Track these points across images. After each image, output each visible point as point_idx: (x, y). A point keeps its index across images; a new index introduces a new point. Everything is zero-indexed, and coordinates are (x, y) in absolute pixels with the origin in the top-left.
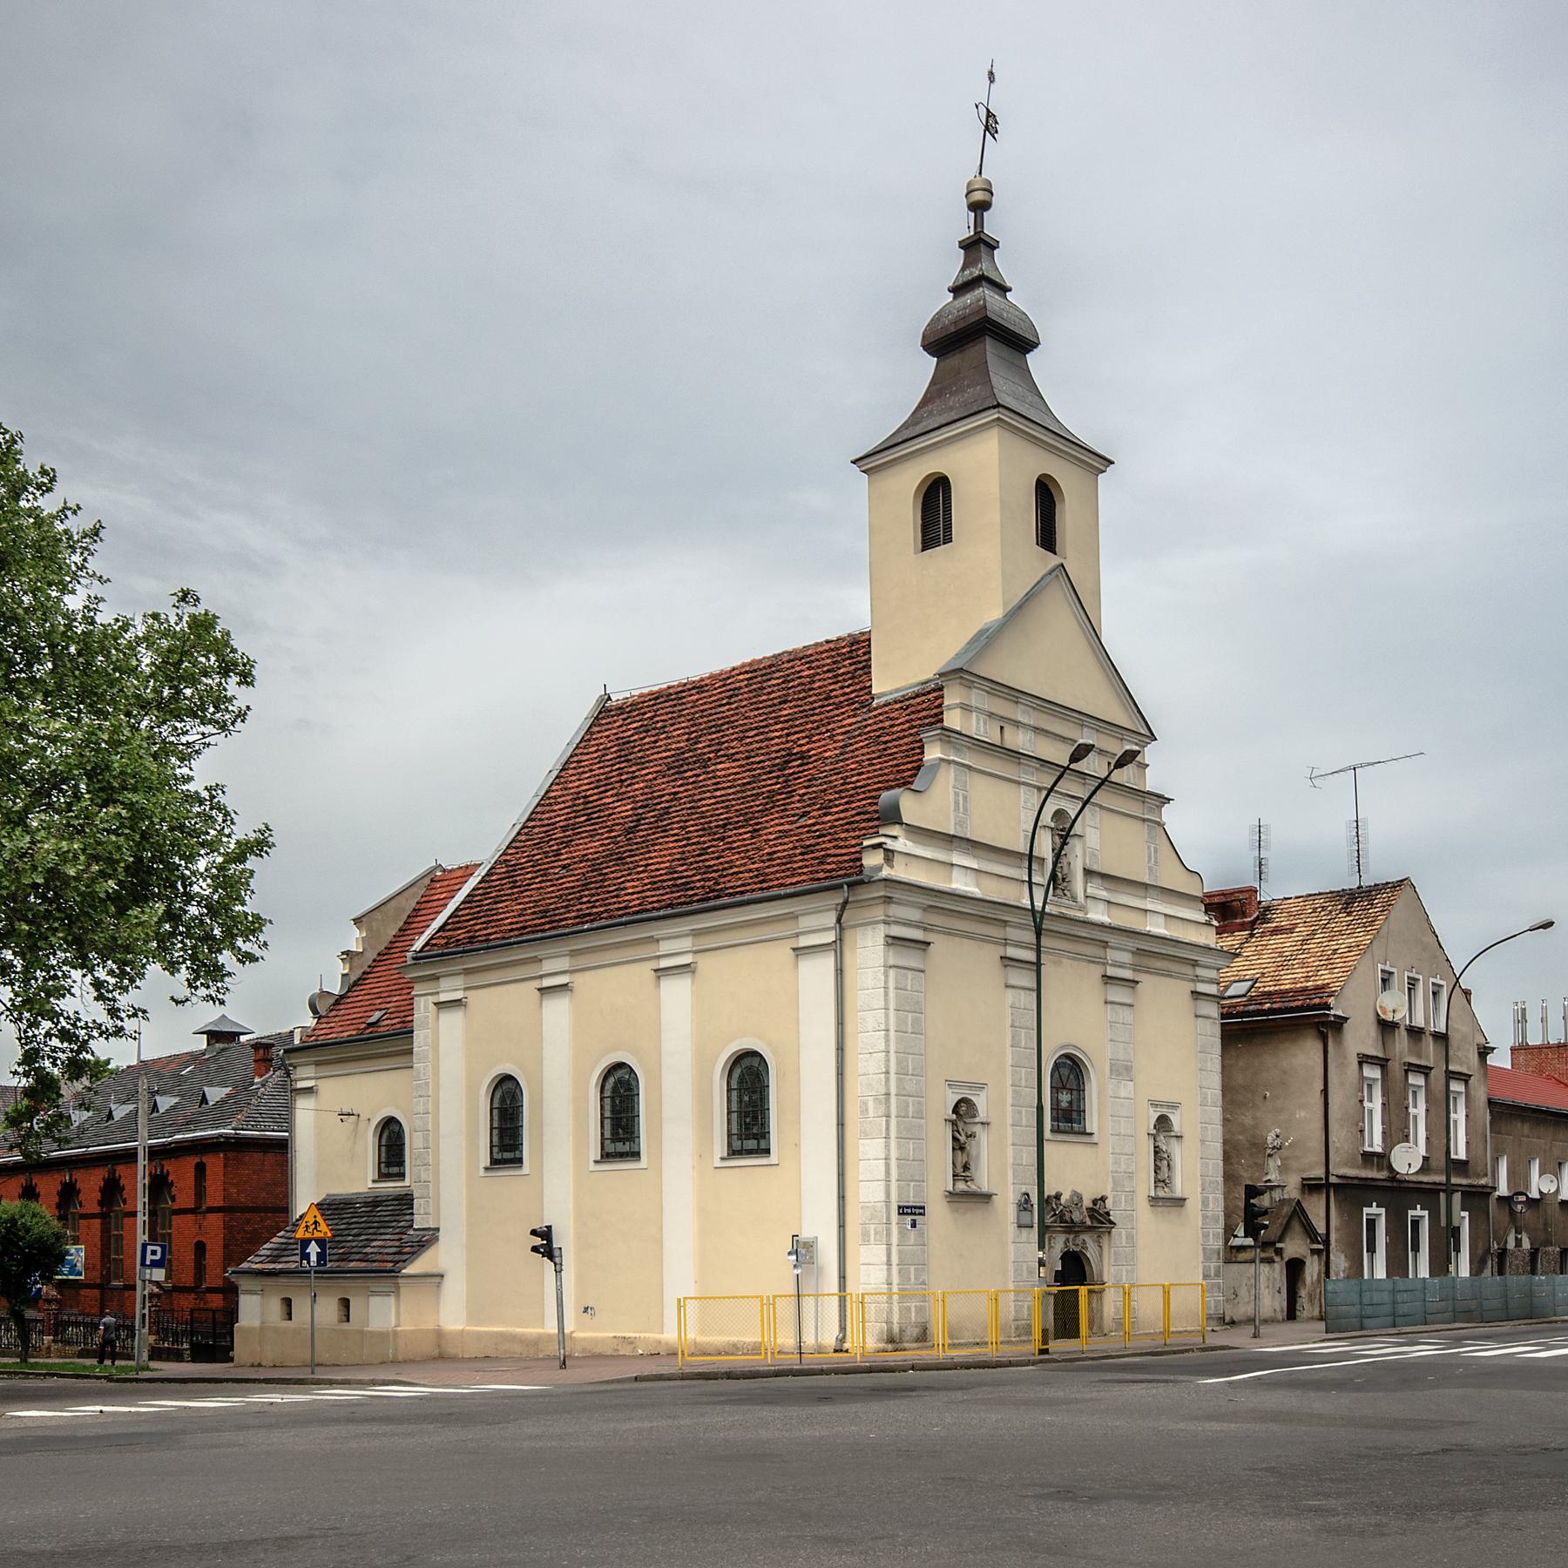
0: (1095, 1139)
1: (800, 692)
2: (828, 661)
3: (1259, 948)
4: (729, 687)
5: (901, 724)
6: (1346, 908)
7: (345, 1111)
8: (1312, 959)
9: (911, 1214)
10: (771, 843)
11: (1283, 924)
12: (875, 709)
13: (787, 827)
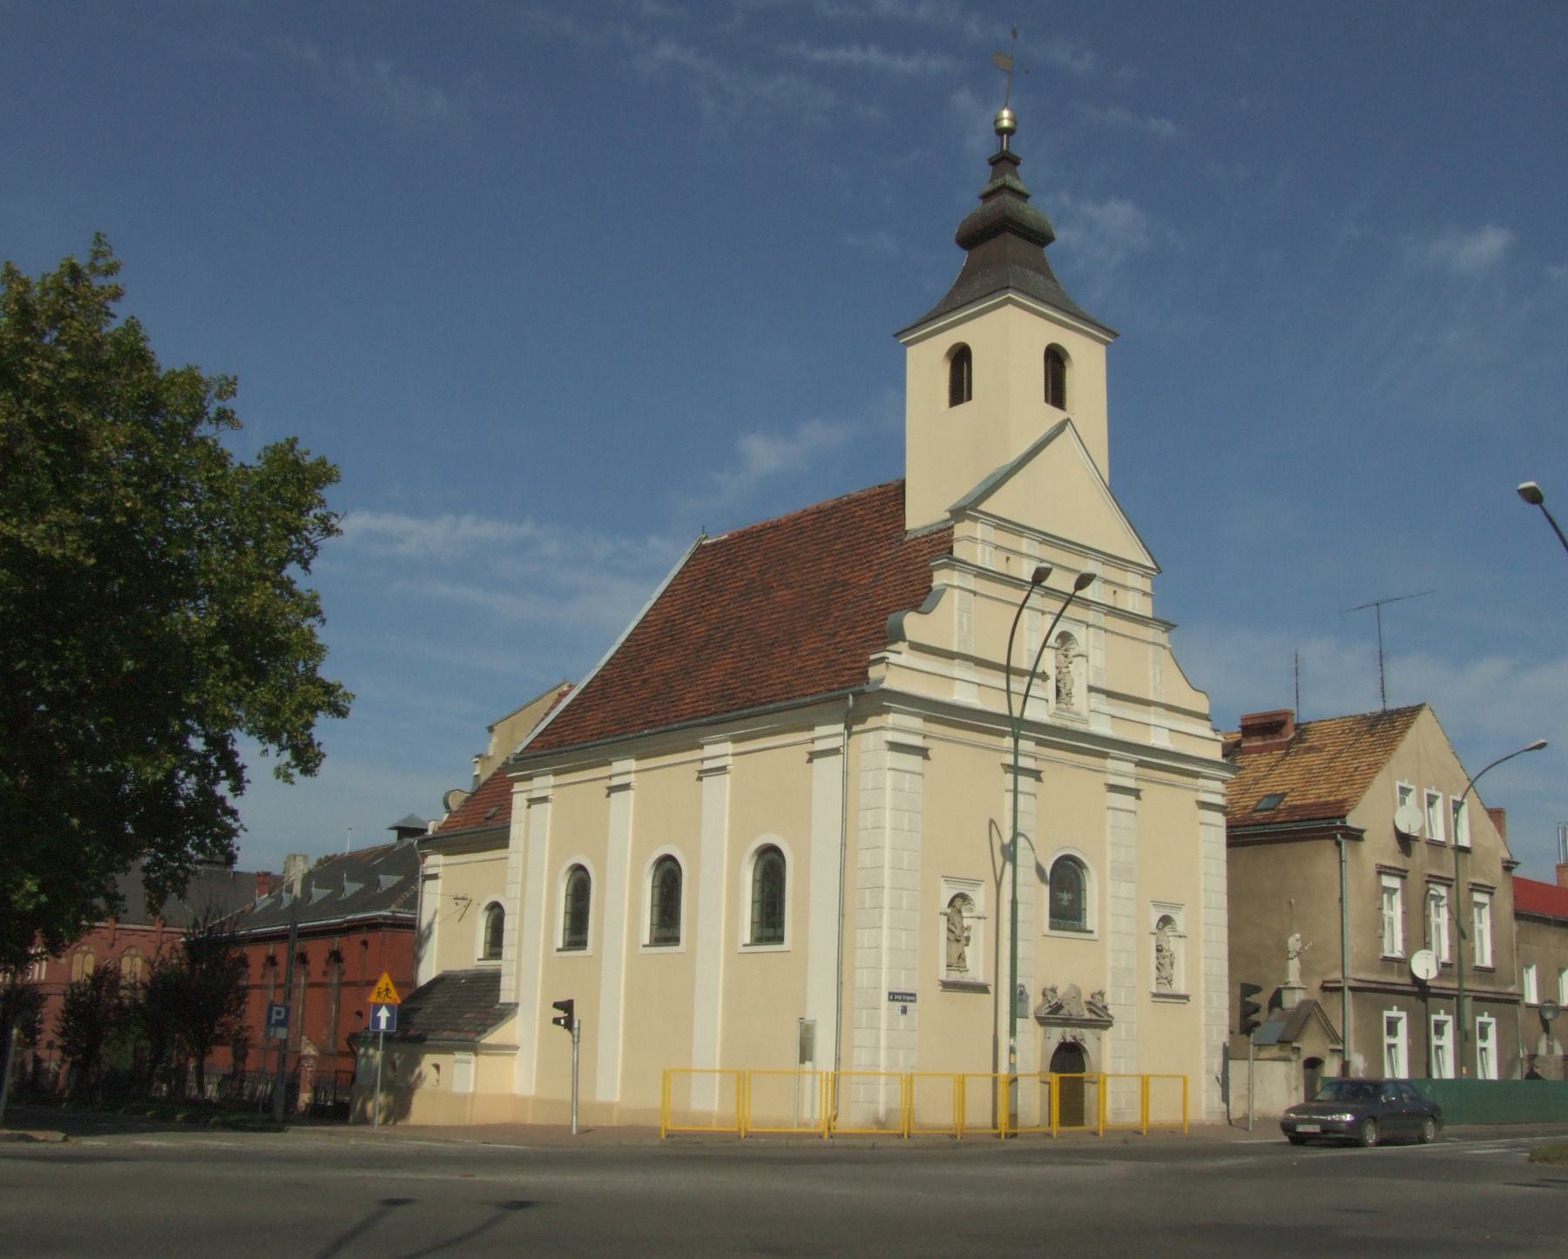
0: (1095, 936)
1: (851, 529)
2: (878, 503)
3: (1293, 765)
4: (798, 526)
5: (924, 555)
6: (1371, 729)
7: (460, 895)
8: (1336, 776)
9: (902, 1000)
10: (803, 659)
11: (1315, 743)
12: (907, 542)
13: (819, 645)
